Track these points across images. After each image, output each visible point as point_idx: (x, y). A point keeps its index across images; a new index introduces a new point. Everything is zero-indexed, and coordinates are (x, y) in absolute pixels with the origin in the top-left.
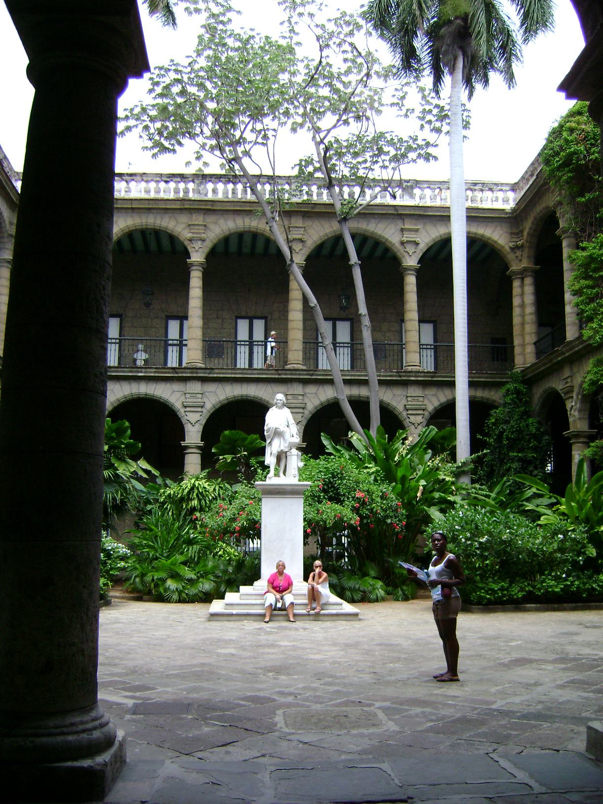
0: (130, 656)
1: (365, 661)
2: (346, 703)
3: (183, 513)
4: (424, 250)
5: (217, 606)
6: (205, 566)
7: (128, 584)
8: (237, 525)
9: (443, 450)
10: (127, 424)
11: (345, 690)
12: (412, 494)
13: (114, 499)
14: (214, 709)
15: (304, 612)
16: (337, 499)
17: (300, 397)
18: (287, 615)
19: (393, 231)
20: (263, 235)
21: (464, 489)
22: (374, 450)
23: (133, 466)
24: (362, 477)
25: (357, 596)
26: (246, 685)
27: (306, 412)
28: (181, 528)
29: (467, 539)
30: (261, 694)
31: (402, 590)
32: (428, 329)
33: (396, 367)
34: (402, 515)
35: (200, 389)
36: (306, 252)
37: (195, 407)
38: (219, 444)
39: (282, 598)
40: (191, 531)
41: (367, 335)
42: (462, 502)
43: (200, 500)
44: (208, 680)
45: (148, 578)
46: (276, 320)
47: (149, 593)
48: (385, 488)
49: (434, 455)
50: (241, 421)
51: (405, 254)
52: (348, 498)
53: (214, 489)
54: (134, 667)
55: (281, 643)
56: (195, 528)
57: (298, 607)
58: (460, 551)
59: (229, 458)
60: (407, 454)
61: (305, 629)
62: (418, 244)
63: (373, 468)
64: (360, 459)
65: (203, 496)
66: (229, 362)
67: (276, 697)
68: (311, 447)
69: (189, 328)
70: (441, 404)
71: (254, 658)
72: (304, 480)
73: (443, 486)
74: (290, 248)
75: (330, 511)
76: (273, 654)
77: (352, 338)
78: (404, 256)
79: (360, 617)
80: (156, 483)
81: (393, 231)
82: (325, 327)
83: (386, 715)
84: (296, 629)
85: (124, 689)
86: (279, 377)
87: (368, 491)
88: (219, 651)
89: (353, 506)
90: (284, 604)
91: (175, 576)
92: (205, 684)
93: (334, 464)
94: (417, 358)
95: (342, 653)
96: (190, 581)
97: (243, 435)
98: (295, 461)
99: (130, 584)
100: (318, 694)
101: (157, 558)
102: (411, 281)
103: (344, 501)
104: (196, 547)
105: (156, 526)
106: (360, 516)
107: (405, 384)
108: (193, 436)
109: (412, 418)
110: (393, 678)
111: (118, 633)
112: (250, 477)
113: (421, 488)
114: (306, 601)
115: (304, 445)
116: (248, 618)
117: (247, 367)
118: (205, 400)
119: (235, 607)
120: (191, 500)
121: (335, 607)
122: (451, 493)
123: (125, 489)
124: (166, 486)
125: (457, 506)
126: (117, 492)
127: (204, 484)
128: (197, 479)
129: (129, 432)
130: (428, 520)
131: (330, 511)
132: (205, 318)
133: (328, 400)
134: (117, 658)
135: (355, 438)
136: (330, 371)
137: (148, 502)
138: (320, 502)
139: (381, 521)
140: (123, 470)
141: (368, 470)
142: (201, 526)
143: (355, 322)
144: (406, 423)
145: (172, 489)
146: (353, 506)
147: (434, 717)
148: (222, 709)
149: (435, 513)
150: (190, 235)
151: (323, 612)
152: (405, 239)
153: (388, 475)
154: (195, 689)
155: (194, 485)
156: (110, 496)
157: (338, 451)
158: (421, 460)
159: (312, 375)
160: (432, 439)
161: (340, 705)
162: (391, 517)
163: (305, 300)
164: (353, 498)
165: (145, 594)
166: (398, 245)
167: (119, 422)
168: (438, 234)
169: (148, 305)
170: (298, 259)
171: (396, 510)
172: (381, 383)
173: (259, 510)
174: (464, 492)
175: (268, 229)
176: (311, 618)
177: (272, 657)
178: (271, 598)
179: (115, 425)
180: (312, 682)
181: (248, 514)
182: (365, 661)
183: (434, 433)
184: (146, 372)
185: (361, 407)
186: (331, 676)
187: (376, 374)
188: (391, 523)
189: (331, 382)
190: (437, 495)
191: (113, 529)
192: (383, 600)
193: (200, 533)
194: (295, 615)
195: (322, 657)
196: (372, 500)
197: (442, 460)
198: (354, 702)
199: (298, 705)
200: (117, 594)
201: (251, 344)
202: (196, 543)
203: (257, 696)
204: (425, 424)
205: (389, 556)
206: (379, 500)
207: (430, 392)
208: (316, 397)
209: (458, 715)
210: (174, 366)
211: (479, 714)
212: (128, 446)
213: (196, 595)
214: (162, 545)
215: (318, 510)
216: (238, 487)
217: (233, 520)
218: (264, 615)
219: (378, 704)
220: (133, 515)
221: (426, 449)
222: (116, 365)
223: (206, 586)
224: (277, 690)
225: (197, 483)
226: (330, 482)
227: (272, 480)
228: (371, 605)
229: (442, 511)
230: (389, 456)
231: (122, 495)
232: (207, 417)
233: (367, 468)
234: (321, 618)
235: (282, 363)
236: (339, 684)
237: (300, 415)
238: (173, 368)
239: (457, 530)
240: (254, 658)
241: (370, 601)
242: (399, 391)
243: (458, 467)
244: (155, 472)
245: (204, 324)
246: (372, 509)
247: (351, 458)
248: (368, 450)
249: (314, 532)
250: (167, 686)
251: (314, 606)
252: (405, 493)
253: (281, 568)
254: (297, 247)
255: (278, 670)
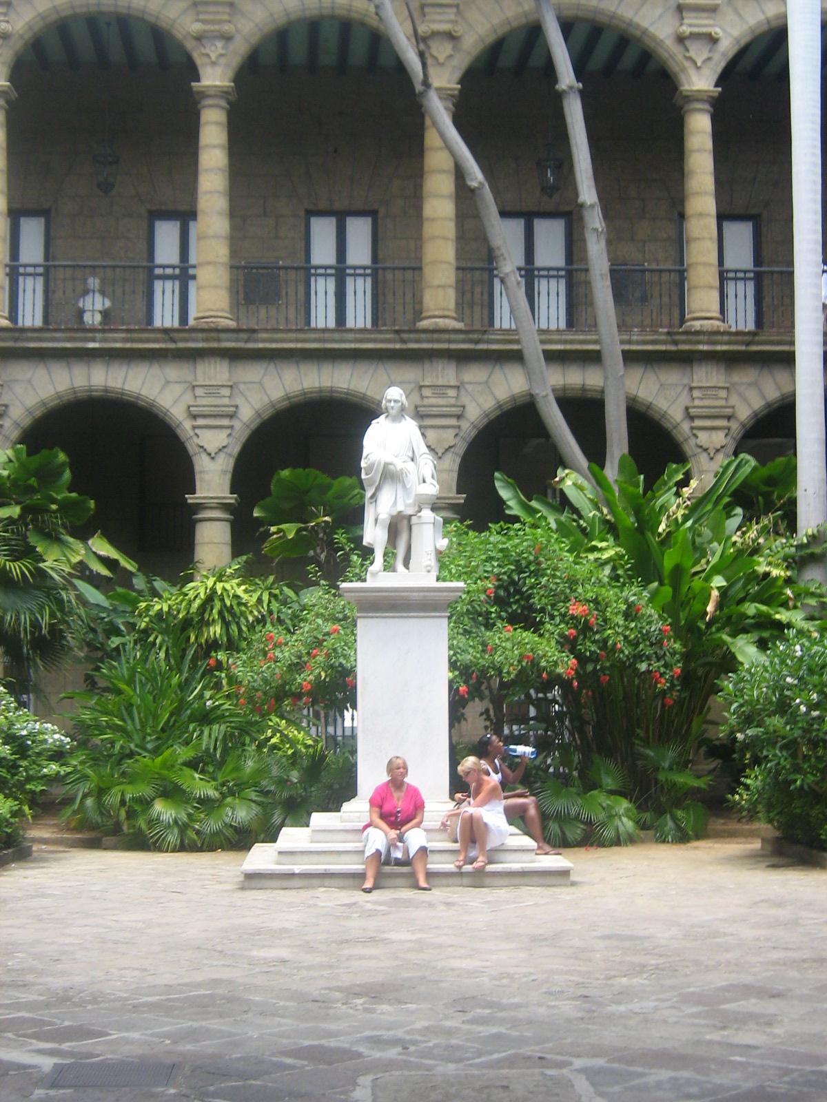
0: (59, 967)
1: (567, 972)
2: (511, 1062)
3: (190, 653)
4: (731, 54)
5: (261, 857)
6: (237, 769)
7: (68, 811)
8: (305, 679)
9: (769, 507)
10: (62, 457)
11: (514, 1033)
12: (696, 606)
13: (35, 625)
14: (226, 1075)
15: (450, 867)
16: (527, 619)
17: (452, 393)
18: (413, 875)
19: (659, 11)
20: (363, 24)
21: (813, 595)
22: (611, 511)
23: (78, 552)
24: (582, 570)
25: (575, 832)
26: (304, 1025)
27: (465, 425)
28: (185, 686)
29: (812, 706)
30: (332, 1043)
31: (674, 819)
32: (740, 237)
33: (665, 320)
34: (673, 654)
35: (226, 376)
36: (461, 62)
37: (212, 415)
38: (268, 500)
39: (401, 838)
40: (208, 694)
41: (597, 252)
42: (806, 625)
43: (226, 625)
44: (221, 1015)
45: (113, 798)
46: (397, 219)
47: (116, 830)
48: (632, 593)
49: (747, 519)
50: (308, 451)
51: (687, 64)
52: (552, 617)
53: (260, 600)
54: (65, 990)
55: (393, 936)
56: (218, 686)
57: (437, 857)
58: (797, 733)
59: (291, 530)
60: (686, 518)
61: (448, 904)
62: (713, 40)
63: (609, 549)
64: (583, 530)
65: (233, 615)
66: (292, 315)
67: (361, 1049)
68: (473, 506)
69: (199, 238)
70: (768, 405)
71: (330, 967)
72: (453, 577)
73: (767, 590)
74: (422, 55)
75: (510, 645)
76: (371, 958)
77: (570, 257)
78: (684, 70)
79: (573, 878)
80: (131, 587)
81: (659, 11)
82: (506, 236)
83: (593, 1084)
84: (431, 905)
85: (37, 1036)
86: (402, 346)
87: (596, 601)
88: (255, 953)
89: (561, 635)
90: (406, 851)
91: (171, 792)
92: (214, 1024)
93: (520, 542)
94: (713, 303)
95: (522, 955)
96: (205, 802)
97: (323, 478)
98: (430, 537)
99: (75, 812)
100: (454, 1042)
101: (131, 755)
102: (700, 126)
103: (542, 623)
104: (218, 730)
105: (131, 682)
106: (580, 657)
107: (686, 359)
108: (213, 480)
109: (703, 438)
110: (622, 1008)
111: (39, 919)
112: (335, 571)
113: (715, 593)
114: (456, 846)
115: (461, 499)
116: (327, 882)
117: (332, 324)
118: (239, 401)
119: (298, 858)
120: (208, 624)
121: (518, 856)
122: (785, 605)
123: (60, 602)
124: (155, 593)
125: (791, 633)
126: (42, 608)
127: (235, 587)
128: (220, 579)
129: (67, 475)
130: (729, 663)
131: (510, 645)
132: (236, 213)
133: (513, 398)
134: (32, 970)
135: (569, 482)
136: (516, 332)
137: (113, 631)
138: (489, 626)
139: (626, 668)
140: (56, 560)
141: (596, 555)
142: (230, 684)
143: (572, 217)
144: (689, 447)
145: (168, 601)
146: (561, 635)
147: (694, 1090)
148: (243, 1075)
149: (746, 650)
150: (196, 27)
151: (490, 868)
152: (686, 30)
153: (643, 565)
154: (191, 1035)
155: (213, 590)
156: (25, 619)
157: (532, 511)
158: (718, 533)
159: (477, 342)
160: (745, 484)
161: (497, 1064)
162: (649, 658)
163: (460, 174)
164: (563, 616)
165: (107, 834)
166: (670, 43)
167: (45, 452)
168: (761, 17)
169: (106, 187)
170: (440, 79)
171: (659, 643)
172: (630, 358)
173: (352, 645)
174: (813, 602)
175: (372, 9)
176: (466, 881)
177: (370, 965)
178: (378, 839)
179: (36, 461)
180: (446, 1017)
181: (328, 656)
182: (567, 972)
183: (746, 470)
184: (104, 340)
185: (585, 413)
186: (490, 1005)
187: (617, 338)
188: (648, 672)
189: (516, 357)
190: (751, 609)
191: (37, 690)
192: (631, 840)
193: (228, 697)
194: (430, 875)
195: (478, 963)
196: (605, 620)
197: (764, 531)
198: (529, 1058)
199: (406, 1065)
200: (45, 834)
201: (341, 273)
202: (220, 719)
203: (322, 1047)
204: (731, 449)
205: (647, 743)
206: (620, 620)
207: (744, 376)
208: (487, 392)
209: (749, 1085)
210: (168, 324)
211: (793, 1083)
212: (65, 506)
213: (218, 833)
214: (143, 726)
215: (484, 644)
216: (312, 596)
217: (297, 667)
218: (361, 876)
219: (578, 1063)
220: (77, 660)
221: (728, 511)
222: (176, 325)
223: (242, 813)
224: (368, 1033)
225: (219, 587)
226: (513, 582)
227: (378, 578)
228: (603, 852)
229: (762, 645)
230: (645, 523)
231: (53, 615)
232: (243, 439)
233: (594, 549)
234: (488, 881)
235: (409, 316)
236: (502, 1021)
237: (452, 432)
238: (166, 331)
239: (790, 687)
240: (330, 967)
241: (602, 844)
242: (672, 377)
243: (800, 547)
244: (127, 564)
245: (234, 228)
246: (605, 641)
247: (562, 529)
248: (598, 509)
249: (475, 692)
250: (133, 1027)
251: (473, 854)
252: (680, 606)
253: (397, 772)
254: (441, 50)
255: (376, 993)
